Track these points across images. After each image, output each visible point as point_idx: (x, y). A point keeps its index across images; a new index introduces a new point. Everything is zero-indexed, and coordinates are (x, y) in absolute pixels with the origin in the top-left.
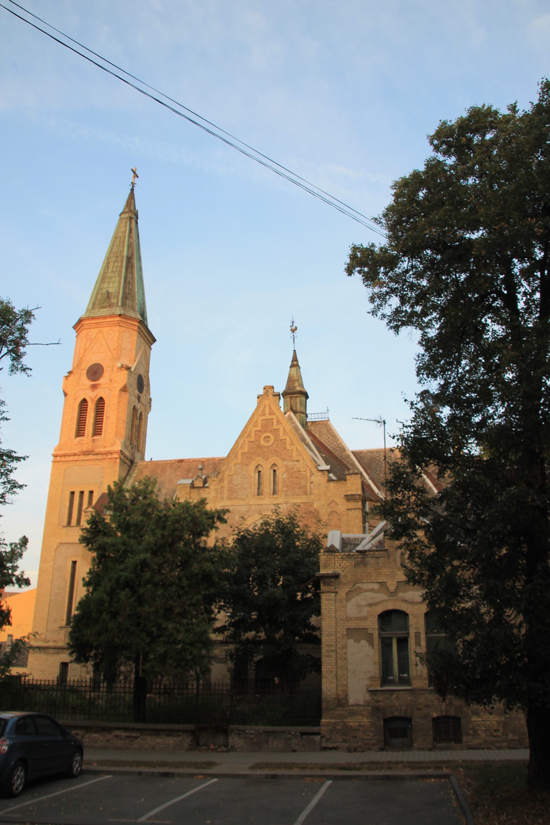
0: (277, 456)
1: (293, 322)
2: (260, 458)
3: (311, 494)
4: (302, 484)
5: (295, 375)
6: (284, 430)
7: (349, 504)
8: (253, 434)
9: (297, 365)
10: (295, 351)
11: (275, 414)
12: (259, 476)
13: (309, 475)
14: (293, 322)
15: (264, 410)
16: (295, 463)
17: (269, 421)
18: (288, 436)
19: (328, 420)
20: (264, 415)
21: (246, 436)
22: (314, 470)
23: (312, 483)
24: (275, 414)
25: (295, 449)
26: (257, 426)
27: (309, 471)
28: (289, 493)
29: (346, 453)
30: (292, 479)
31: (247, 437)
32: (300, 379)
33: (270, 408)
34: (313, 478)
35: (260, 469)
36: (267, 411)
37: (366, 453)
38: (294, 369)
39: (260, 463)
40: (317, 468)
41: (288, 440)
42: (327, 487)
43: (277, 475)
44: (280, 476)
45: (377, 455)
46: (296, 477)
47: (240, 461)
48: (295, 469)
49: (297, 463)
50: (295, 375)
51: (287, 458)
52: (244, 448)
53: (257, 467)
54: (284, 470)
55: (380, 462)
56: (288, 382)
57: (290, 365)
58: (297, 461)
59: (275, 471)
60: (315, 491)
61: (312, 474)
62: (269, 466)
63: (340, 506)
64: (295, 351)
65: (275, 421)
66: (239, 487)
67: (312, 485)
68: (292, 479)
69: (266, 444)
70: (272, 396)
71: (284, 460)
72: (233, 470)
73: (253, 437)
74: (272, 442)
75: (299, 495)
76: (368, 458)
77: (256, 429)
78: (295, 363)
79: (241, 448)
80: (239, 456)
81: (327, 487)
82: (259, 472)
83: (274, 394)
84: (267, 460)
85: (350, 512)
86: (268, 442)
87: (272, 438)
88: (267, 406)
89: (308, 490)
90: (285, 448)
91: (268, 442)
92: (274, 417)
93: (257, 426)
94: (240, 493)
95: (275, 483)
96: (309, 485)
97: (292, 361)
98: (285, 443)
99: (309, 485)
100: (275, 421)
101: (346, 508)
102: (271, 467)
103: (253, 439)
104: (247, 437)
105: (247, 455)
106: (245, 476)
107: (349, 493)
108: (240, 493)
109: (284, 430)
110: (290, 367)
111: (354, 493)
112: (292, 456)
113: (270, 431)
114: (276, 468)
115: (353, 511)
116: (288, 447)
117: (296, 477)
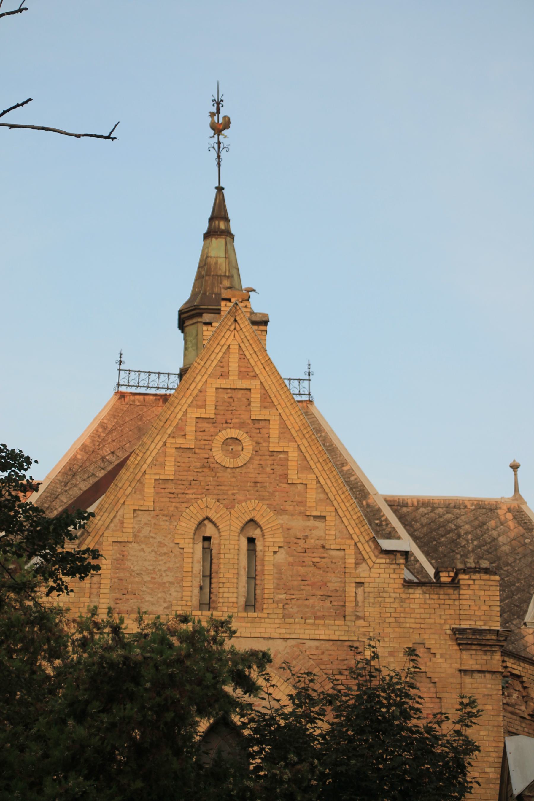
0: (261, 499)
1: (218, 103)
2: (210, 500)
3: (358, 618)
4: (332, 586)
5: (222, 261)
6: (283, 425)
7: (465, 655)
8: (190, 428)
9: (228, 234)
10: (220, 189)
11: (256, 376)
12: (207, 551)
13: (351, 560)
14: (218, 103)
15: (223, 363)
16: (312, 523)
17: (240, 394)
18: (294, 445)
19: (310, 401)
20: (223, 375)
21: (169, 431)
22: (367, 549)
23: (360, 584)
24: (256, 376)
25: (312, 485)
26: (204, 406)
27: (351, 551)
28: (292, 609)
29: (370, 501)
30: (302, 570)
31: (172, 436)
32: (234, 272)
33: (242, 356)
34: (363, 571)
35: (210, 530)
36: (234, 365)
37: (417, 508)
38: (218, 244)
39: (211, 514)
40: (377, 545)
41: (293, 455)
42: (402, 601)
43: (259, 554)
44: (269, 558)
45: (448, 516)
46: (314, 564)
47: (149, 504)
48: (311, 542)
49: (317, 523)
50: (222, 261)
51: (291, 508)
52: (163, 465)
53: (200, 524)
54: (280, 539)
55: (459, 536)
56: (200, 277)
57: (205, 230)
58: (315, 517)
59: (251, 541)
60: (369, 611)
61: (360, 560)
62: (238, 525)
63: (439, 660)
64: (220, 189)
65: (255, 397)
66: (147, 578)
67: (360, 590)
68: (302, 570)
69: (228, 462)
70: (247, 322)
71: (279, 511)
72: (130, 525)
73: (191, 436)
74: (245, 456)
75: (323, 618)
76: (424, 520)
77: (201, 413)
78: (222, 226)
79: (153, 464)
80: (149, 489)
81: (402, 601)
82: (207, 539)
83: (254, 319)
84: (229, 507)
85: (468, 680)
86: (235, 455)
87: (248, 443)
88: (234, 349)
89: (350, 604)
90: (286, 476)
91: (235, 455)
92: (254, 384)
93: (204, 406)
94: (148, 598)
95: (252, 577)
96: (351, 589)
97: (211, 220)
98: (284, 463)
99: (351, 589)
100: (255, 397)
101: (457, 666)
102: (243, 529)
103: (190, 442)
104: (172, 436)
105: (171, 487)
106: (164, 550)
107: (465, 625)
108: (148, 598)
109: (283, 425)
110: (207, 236)
111: (480, 625)
112: (302, 503)
113: (241, 425)
114: (256, 533)
115: (477, 676)
116: (293, 475)
117: (314, 564)
